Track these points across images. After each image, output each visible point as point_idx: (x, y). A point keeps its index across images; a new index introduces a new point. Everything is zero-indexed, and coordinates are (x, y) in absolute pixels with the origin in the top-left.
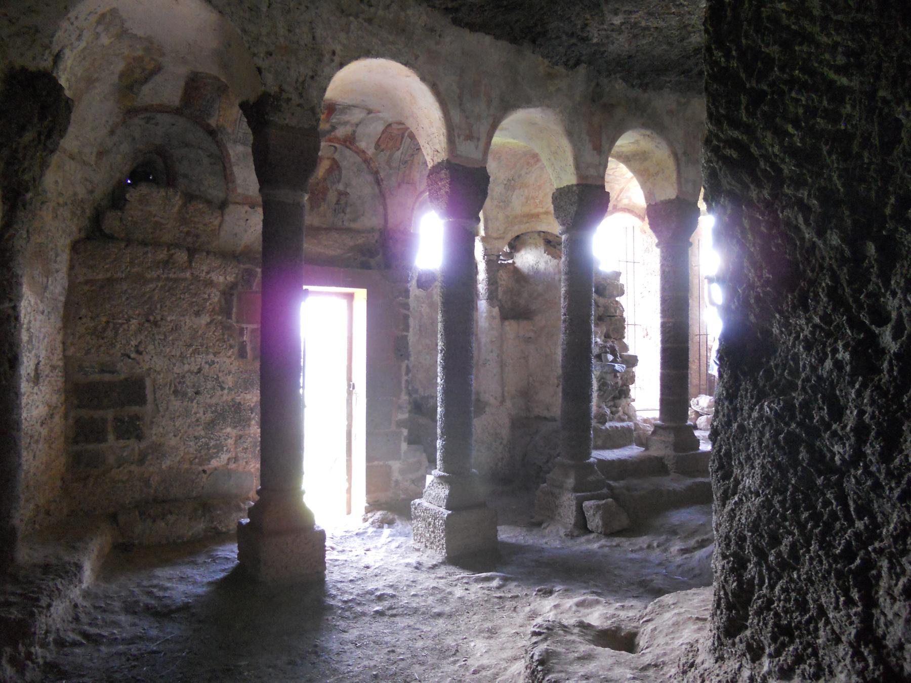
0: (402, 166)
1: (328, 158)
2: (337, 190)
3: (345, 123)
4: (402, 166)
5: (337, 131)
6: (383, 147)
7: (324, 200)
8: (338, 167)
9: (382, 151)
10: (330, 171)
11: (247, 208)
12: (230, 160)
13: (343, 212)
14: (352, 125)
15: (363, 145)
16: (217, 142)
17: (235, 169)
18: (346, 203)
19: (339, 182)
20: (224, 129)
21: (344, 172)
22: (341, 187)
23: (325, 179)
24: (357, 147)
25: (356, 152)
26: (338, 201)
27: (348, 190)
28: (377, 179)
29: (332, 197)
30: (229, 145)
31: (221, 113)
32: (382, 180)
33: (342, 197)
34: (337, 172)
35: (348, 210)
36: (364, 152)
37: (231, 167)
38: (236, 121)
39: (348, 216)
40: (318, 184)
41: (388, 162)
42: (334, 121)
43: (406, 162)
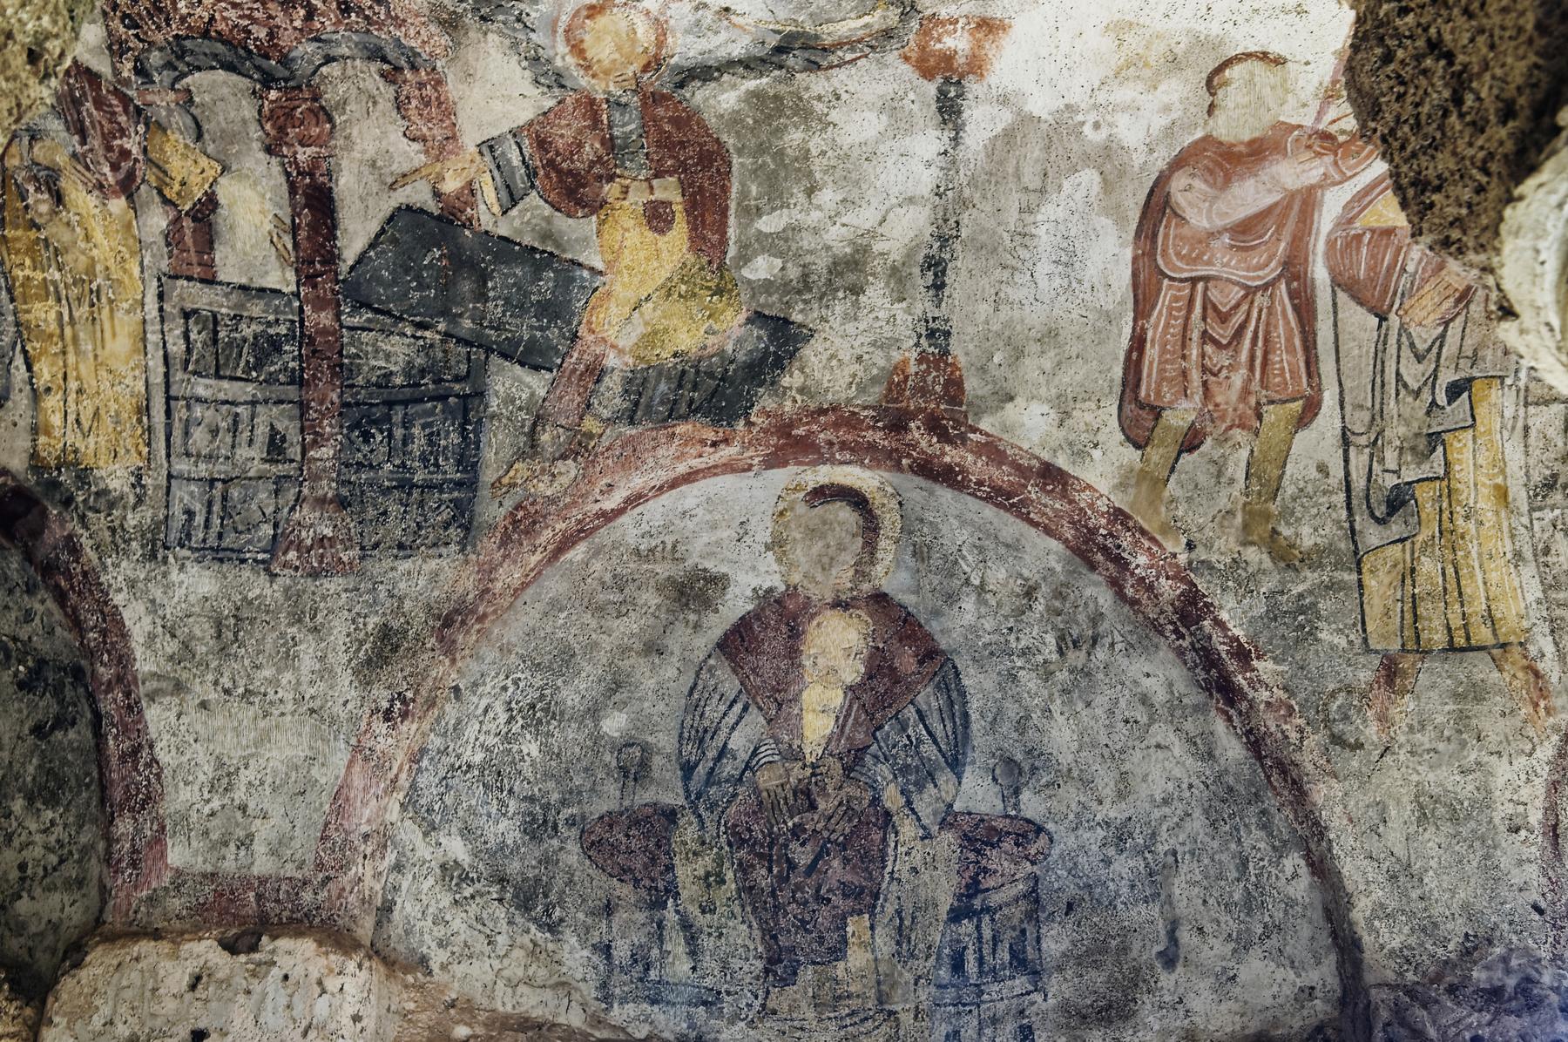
0: (1372, 535)
1: (839, 604)
2: (948, 819)
3: (849, 271)
4: (1372, 535)
5: (813, 354)
6: (1181, 415)
7: (865, 898)
8: (930, 654)
9: (1191, 441)
10: (878, 690)
11: (205, 951)
12: (124, 660)
13: (1019, 961)
14: (1018, 468)
15: (1029, 425)
16: (49, 569)
17: (156, 717)
18: (1033, 897)
19: (956, 764)
20: (84, 476)
21: (978, 683)
22: (977, 792)
23: (853, 761)
24: (992, 451)
25: (999, 496)
26: (974, 888)
27: (1032, 805)
28: (1208, 658)
29: (923, 867)
30: (119, 574)
31: (45, 372)
32: (1242, 656)
33: (997, 860)
34: (928, 697)
35: (1055, 941)
36: (1050, 475)
37: (133, 708)
38: (144, 410)
39: (1059, 988)
40: (806, 797)
41: (1261, 521)
42: (762, 268)
43: (1398, 501)
